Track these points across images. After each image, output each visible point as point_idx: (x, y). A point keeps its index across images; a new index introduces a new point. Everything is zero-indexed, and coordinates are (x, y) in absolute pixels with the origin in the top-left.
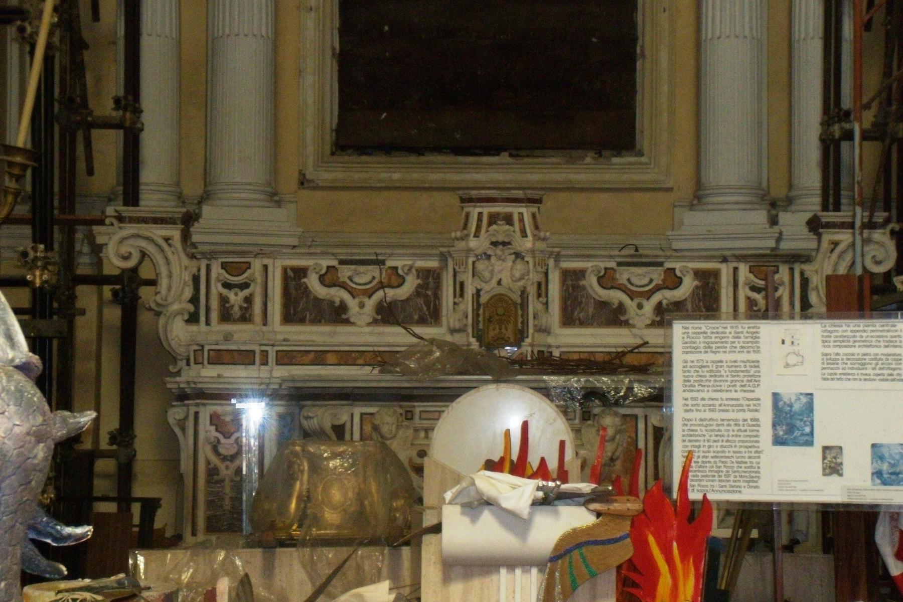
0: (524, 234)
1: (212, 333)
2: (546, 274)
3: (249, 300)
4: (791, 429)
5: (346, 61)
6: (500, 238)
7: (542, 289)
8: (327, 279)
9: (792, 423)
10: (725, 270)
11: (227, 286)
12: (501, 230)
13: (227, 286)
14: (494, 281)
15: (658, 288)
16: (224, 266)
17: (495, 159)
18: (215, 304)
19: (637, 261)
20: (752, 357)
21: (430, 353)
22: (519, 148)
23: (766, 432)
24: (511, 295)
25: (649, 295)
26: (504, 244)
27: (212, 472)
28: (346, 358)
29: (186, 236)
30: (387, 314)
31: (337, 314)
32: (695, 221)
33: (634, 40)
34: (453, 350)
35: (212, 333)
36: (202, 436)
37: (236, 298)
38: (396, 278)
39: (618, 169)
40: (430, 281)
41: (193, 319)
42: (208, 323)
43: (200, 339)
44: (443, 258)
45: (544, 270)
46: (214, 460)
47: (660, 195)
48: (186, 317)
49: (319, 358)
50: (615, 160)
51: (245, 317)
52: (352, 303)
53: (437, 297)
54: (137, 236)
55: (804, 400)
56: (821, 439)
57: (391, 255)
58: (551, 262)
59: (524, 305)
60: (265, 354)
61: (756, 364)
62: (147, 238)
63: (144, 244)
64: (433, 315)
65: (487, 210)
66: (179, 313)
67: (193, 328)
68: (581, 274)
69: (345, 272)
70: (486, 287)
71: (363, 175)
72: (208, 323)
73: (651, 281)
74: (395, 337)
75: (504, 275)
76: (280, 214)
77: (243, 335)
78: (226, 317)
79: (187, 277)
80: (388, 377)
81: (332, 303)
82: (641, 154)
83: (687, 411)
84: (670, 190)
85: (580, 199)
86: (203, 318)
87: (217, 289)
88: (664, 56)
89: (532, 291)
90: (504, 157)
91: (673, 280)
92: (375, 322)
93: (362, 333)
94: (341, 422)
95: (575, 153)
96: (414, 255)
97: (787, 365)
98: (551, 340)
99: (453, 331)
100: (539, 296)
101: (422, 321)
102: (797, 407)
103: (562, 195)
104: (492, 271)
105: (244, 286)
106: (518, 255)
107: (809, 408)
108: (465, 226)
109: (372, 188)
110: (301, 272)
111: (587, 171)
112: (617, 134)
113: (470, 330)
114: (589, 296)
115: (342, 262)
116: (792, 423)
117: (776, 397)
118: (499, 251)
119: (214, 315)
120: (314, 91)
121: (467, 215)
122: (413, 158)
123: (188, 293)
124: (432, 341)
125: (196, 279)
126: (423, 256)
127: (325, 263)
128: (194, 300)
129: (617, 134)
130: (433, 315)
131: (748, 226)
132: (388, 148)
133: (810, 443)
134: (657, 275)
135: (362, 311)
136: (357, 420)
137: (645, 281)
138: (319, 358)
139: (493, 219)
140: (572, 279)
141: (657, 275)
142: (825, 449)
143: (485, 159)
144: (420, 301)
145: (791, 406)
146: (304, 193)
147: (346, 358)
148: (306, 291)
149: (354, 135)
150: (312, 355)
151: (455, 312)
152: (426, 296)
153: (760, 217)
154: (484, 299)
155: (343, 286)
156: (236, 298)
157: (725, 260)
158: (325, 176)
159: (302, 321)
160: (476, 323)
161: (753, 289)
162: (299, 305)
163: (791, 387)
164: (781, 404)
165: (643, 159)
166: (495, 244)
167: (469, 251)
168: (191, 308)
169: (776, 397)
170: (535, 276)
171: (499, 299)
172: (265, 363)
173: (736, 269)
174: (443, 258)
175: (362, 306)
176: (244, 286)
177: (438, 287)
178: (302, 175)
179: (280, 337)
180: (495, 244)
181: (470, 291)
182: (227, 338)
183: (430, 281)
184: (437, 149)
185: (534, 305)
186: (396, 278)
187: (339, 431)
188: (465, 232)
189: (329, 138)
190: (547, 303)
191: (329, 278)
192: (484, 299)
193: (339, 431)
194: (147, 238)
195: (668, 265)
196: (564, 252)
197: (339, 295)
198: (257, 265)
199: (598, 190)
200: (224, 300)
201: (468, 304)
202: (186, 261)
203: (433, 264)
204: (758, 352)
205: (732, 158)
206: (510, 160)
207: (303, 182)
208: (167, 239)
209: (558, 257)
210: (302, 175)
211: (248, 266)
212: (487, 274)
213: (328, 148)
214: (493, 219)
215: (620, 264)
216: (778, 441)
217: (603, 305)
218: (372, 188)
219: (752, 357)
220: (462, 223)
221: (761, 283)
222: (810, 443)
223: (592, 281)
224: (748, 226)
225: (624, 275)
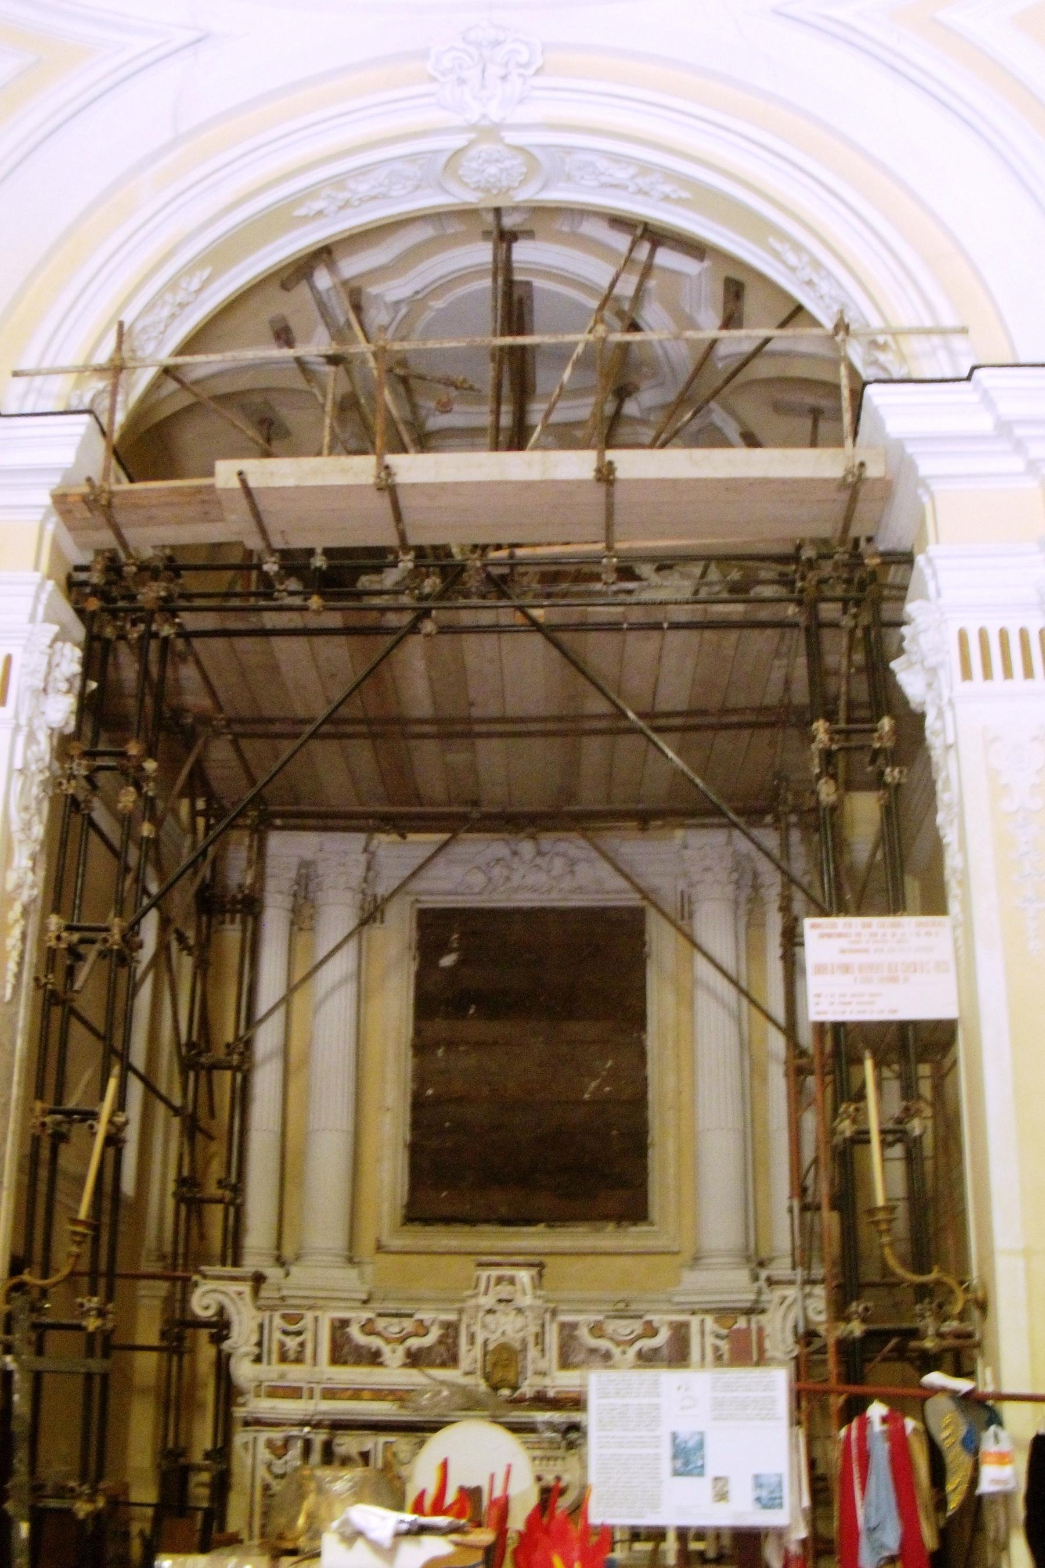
0: (524, 1293)
1: (271, 1371)
2: (543, 1326)
3: (302, 1345)
4: (686, 1463)
5: (415, 1150)
6: (504, 1296)
7: (540, 1338)
8: (367, 1328)
9: (687, 1458)
10: (695, 1321)
11: (286, 1333)
12: (505, 1290)
13: (286, 1333)
14: (498, 1333)
15: (639, 1337)
16: (284, 1317)
17: (532, 1229)
18: (275, 1347)
19: (620, 1315)
20: (654, 1401)
21: (439, 1392)
22: (556, 1219)
23: (666, 1464)
24: (513, 1343)
25: (632, 1342)
26: (509, 1301)
27: (266, 1488)
28: (379, 1395)
29: (256, 1292)
30: (415, 1359)
31: (374, 1358)
32: (691, 1279)
33: (646, 1132)
34: (462, 1389)
35: (271, 1371)
36: (259, 1457)
37: (292, 1343)
38: (422, 1329)
39: (633, 1237)
40: (451, 1329)
41: (258, 1359)
42: (269, 1363)
43: (263, 1377)
44: (460, 1311)
45: (540, 1322)
46: (269, 1479)
47: (668, 1258)
48: (252, 1358)
49: (356, 1394)
50: (633, 1229)
51: (299, 1360)
52: (386, 1349)
53: (456, 1344)
54: (214, 1291)
55: (697, 1438)
56: (712, 1469)
57: (418, 1309)
58: (548, 1316)
59: (525, 1348)
60: (311, 1390)
61: (657, 1407)
62: (223, 1293)
63: (221, 1298)
64: (452, 1360)
65: (495, 1272)
66: (247, 1354)
67: (258, 1367)
68: (574, 1326)
69: (381, 1324)
70: (493, 1337)
71: (427, 1242)
72: (269, 1363)
73: (632, 1332)
74: (414, 1377)
75: (508, 1327)
76: (353, 1273)
77: (296, 1374)
78: (283, 1358)
79: (254, 1325)
80: (403, 1412)
81: (369, 1349)
82: (652, 1224)
83: (601, 1447)
84: (676, 1253)
85: (603, 1260)
86: (265, 1359)
87: (277, 1335)
88: (671, 1147)
89: (531, 1340)
90: (541, 1227)
91: (651, 1331)
92: (405, 1365)
93: (393, 1374)
94: (366, 1449)
95: (599, 1224)
96: (437, 1310)
97: (683, 1408)
98: (547, 1381)
99: (467, 1374)
100: (537, 1344)
101: (443, 1365)
102: (691, 1444)
103: (590, 1259)
104: (497, 1323)
105: (299, 1333)
106: (520, 1311)
107: (701, 1445)
108: (476, 1286)
109: (435, 1253)
110: (345, 1323)
111: (609, 1237)
112: (635, 1211)
113: (479, 1373)
114: (581, 1345)
115: (380, 1315)
116: (687, 1458)
117: (674, 1436)
118: (502, 1306)
119: (275, 1356)
120: (389, 1174)
121: (478, 1279)
122: (467, 1228)
123: (254, 1338)
124: (443, 1383)
125: (261, 1327)
126: (446, 1310)
127: (366, 1315)
128: (259, 1344)
129: (635, 1211)
130: (452, 1360)
131: (734, 1283)
132: (448, 1220)
133: (701, 1474)
134: (637, 1326)
135: (394, 1355)
136: (380, 1447)
137: (628, 1331)
138: (356, 1394)
139: (500, 1280)
140: (568, 1331)
141: (637, 1326)
142: (716, 1479)
143: (525, 1229)
144: (442, 1349)
145: (686, 1442)
146: (381, 1258)
147: (379, 1395)
148: (348, 1339)
149: (418, 1213)
150: (349, 1393)
151: (469, 1355)
152: (447, 1344)
153: (742, 1276)
154: (491, 1347)
155: (378, 1334)
156: (292, 1343)
157: (693, 1313)
158: (396, 1243)
159: (345, 1363)
160: (484, 1367)
161: (718, 1336)
162: (343, 1351)
163: (686, 1428)
164: (678, 1441)
165: (655, 1228)
166: (500, 1301)
167: (478, 1307)
168: (256, 1350)
169: (674, 1436)
170: (533, 1329)
171: (503, 1348)
172: (311, 1397)
173: (703, 1321)
174: (460, 1311)
175: (394, 1351)
176: (299, 1333)
177: (456, 1336)
178: (378, 1241)
179: (325, 1377)
180: (500, 1301)
181: (479, 1340)
182: (282, 1376)
183: (451, 1329)
184: (487, 1221)
185: (533, 1352)
186: (422, 1329)
187: (365, 1456)
188: (476, 1291)
189: (400, 1213)
190: (543, 1350)
191: (368, 1328)
192: (491, 1347)
193: (365, 1456)
194: (223, 1293)
195: (648, 1317)
196: (563, 1307)
197: (375, 1342)
198: (309, 1316)
199: (620, 1254)
200: (282, 1345)
201: (478, 1351)
202: (254, 1312)
203: (452, 1317)
204: (658, 1396)
205: (720, 1226)
206: (547, 1230)
207: (380, 1248)
208: (240, 1294)
209: (554, 1313)
210: (378, 1241)
211: (301, 1317)
212: (493, 1327)
213: (399, 1219)
214: (500, 1280)
215: (608, 1317)
216: (677, 1473)
217: (593, 1351)
218: (435, 1253)
219: (654, 1401)
220: (473, 1284)
221: (725, 1332)
222: (701, 1474)
223: (583, 1333)
224: (734, 1283)
225: (611, 1326)
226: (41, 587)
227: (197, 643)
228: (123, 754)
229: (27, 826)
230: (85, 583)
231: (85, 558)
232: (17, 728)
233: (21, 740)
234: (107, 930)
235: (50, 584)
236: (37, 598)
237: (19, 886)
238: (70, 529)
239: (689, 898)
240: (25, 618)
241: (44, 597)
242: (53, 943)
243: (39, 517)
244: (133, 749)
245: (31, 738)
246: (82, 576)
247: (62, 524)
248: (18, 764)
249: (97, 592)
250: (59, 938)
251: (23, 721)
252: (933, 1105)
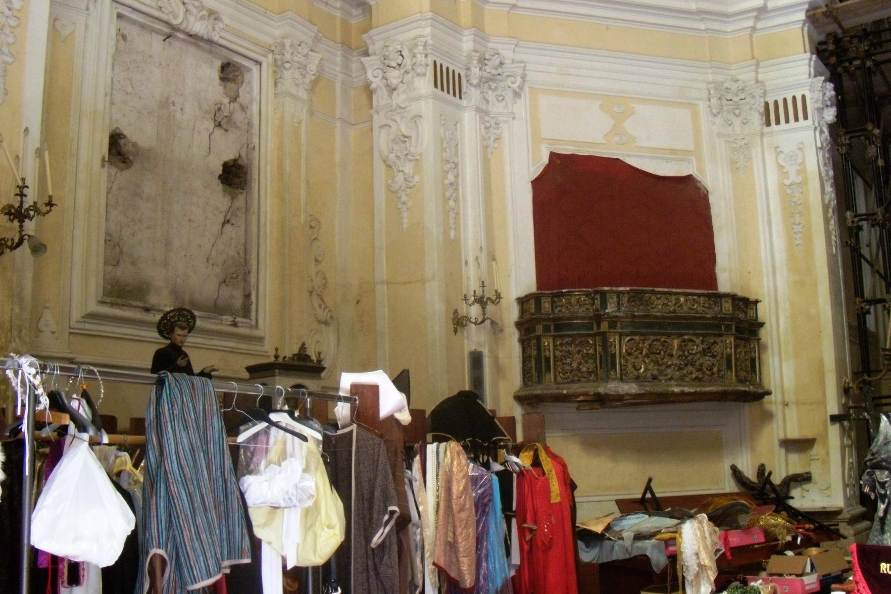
45: (283, 504)
226: (810, 59)
227: (883, 66)
228: (865, 130)
229: (827, 172)
230: (825, 50)
231: (822, 38)
232: (815, 129)
233: (818, 133)
234: (875, 214)
235: (814, 57)
236: (810, 66)
237: (830, 201)
238: (816, 27)
239: (436, 86)
240: (807, 76)
241: (812, 63)
242: (850, 224)
243: (801, 25)
244: (870, 127)
245: (822, 132)
246: (824, 47)
247: (812, 27)
248: (819, 145)
249: (832, 53)
250: (853, 222)
251: (817, 124)
252: (861, 256)
